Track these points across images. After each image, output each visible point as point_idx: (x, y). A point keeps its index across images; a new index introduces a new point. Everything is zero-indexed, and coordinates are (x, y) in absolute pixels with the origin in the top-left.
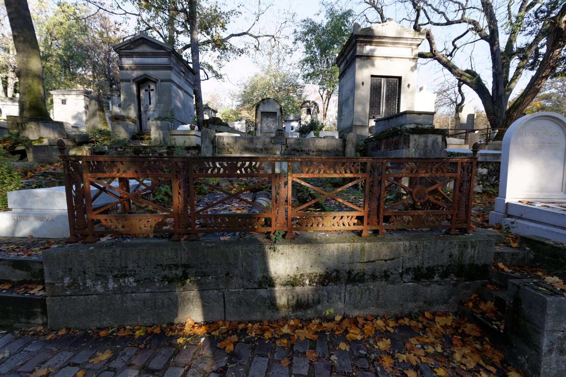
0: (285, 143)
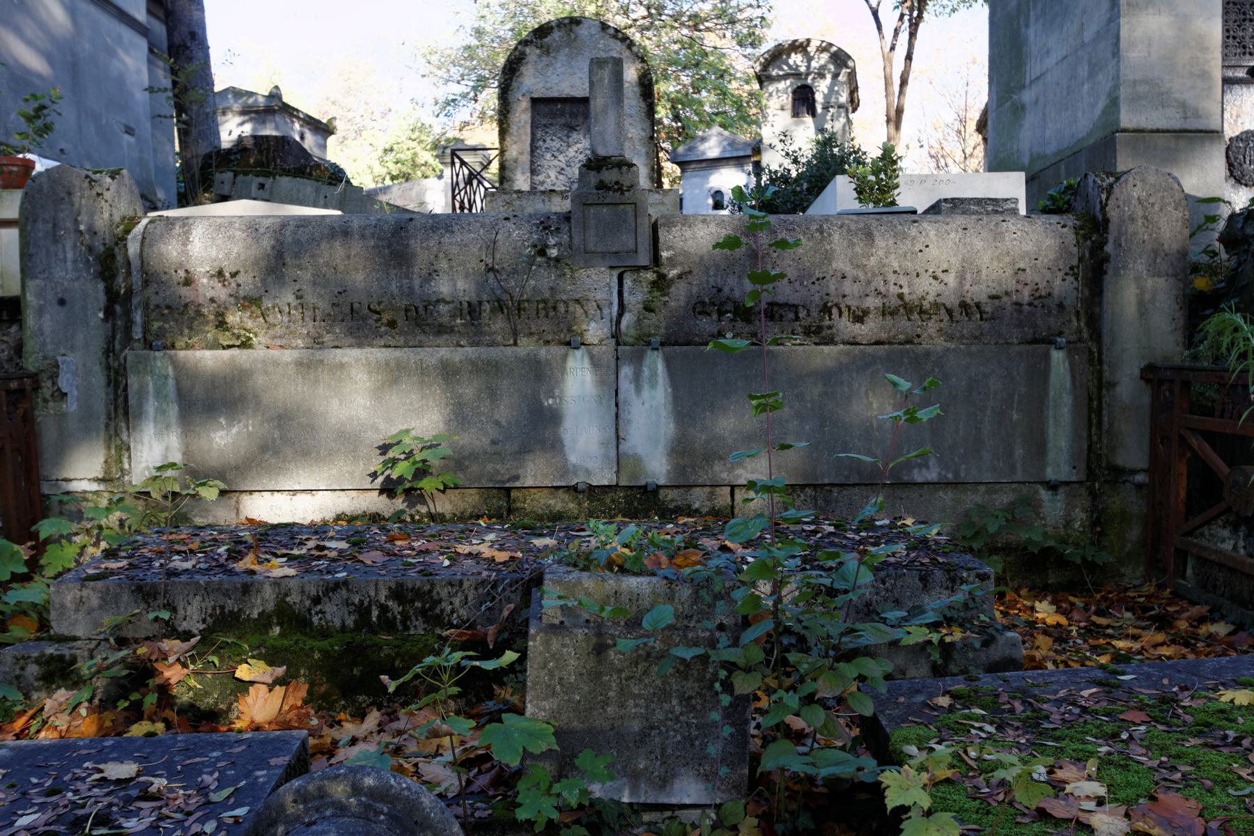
0: (644, 259)
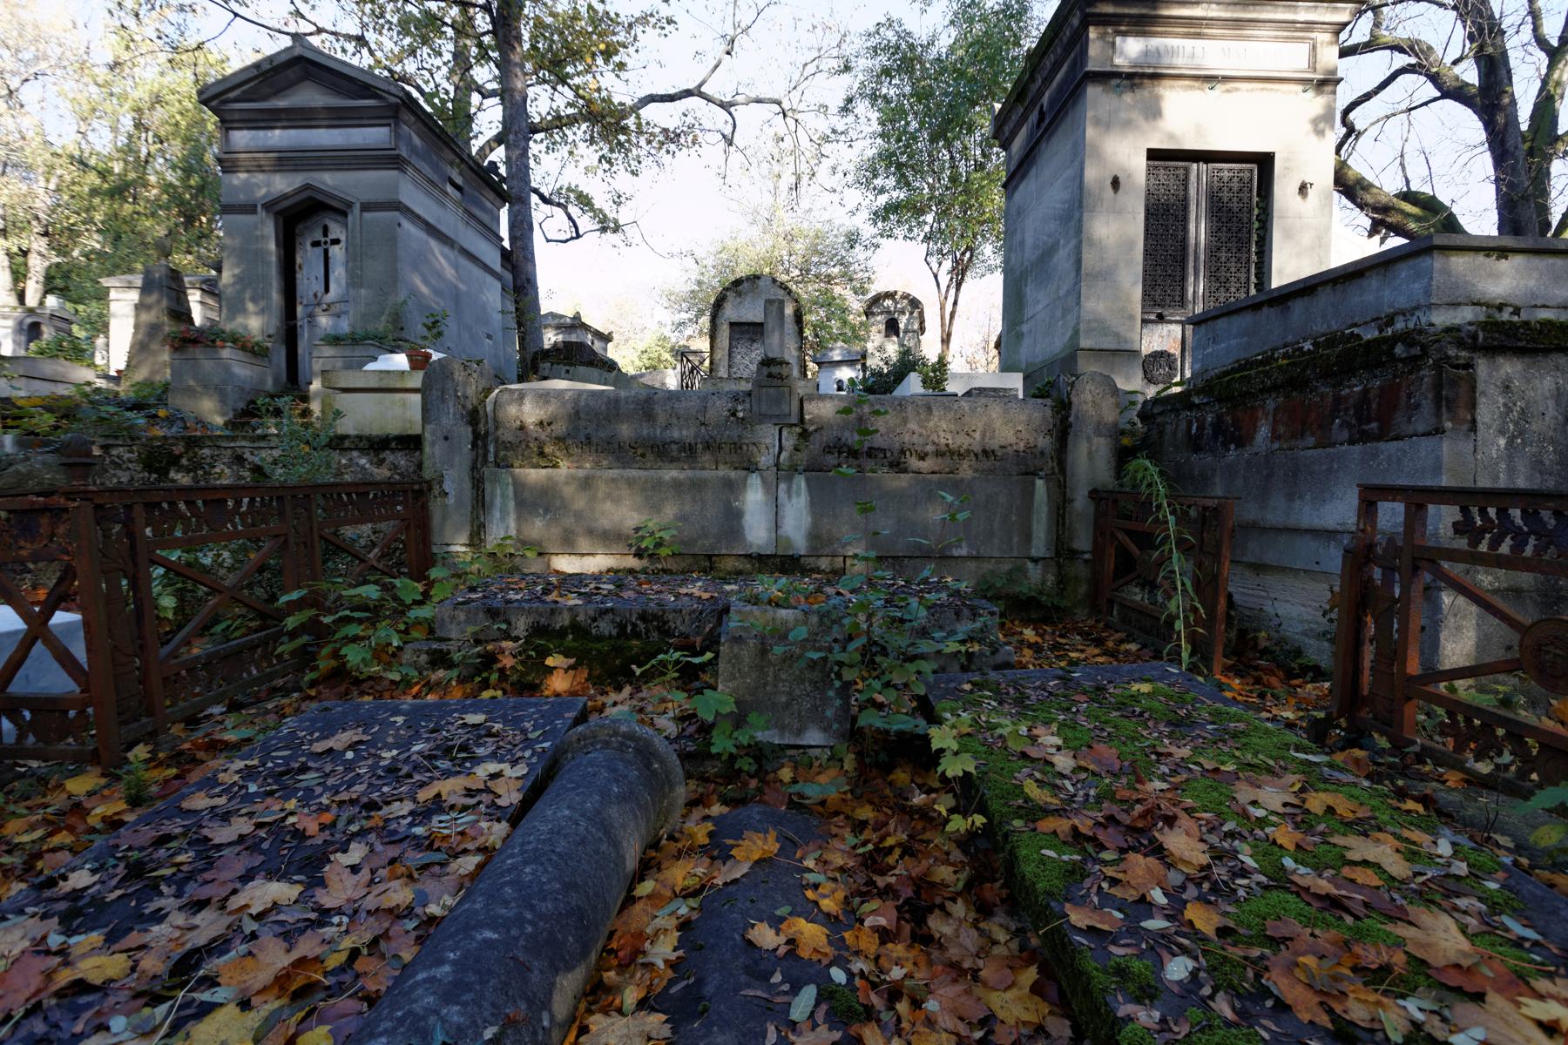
0: (794, 420)
